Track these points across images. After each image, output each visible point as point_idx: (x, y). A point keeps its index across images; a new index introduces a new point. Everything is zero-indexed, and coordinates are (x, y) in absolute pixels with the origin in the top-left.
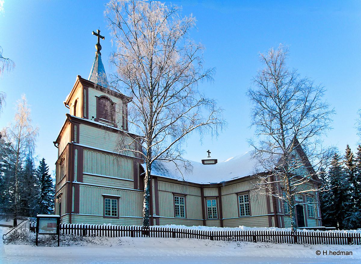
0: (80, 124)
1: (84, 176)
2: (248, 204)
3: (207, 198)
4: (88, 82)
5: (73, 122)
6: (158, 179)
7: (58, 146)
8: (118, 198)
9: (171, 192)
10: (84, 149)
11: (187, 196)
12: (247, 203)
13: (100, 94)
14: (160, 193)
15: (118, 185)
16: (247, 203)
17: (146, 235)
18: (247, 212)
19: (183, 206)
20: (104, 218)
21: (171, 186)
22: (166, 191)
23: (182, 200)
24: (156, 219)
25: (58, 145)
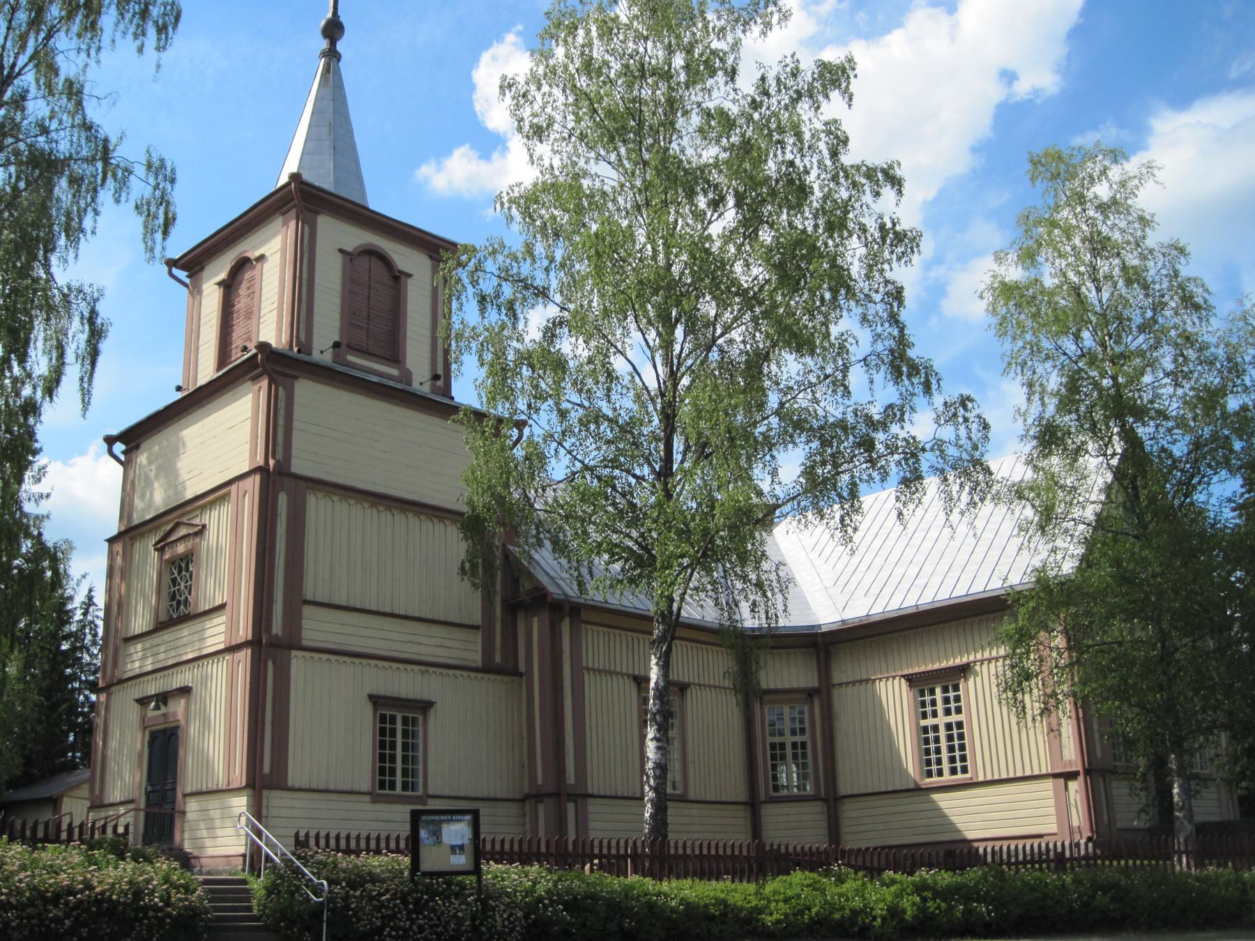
0: (296, 378)
1: (307, 611)
2: (924, 716)
3: (766, 697)
4: (319, 193)
5: (274, 371)
6: (585, 615)
7: (122, 458)
8: (425, 706)
9: (628, 676)
10: (308, 491)
11: (689, 691)
12: (930, 722)
13: (356, 237)
14: (590, 682)
15: (429, 643)
16: (930, 722)
17: (783, 850)
18: (952, 760)
19: (804, 745)
20: (373, 802)
21: (607, 639)
22: (605, 672)
23: (931, 735)
24: (575, 802)
25: (124, 452)
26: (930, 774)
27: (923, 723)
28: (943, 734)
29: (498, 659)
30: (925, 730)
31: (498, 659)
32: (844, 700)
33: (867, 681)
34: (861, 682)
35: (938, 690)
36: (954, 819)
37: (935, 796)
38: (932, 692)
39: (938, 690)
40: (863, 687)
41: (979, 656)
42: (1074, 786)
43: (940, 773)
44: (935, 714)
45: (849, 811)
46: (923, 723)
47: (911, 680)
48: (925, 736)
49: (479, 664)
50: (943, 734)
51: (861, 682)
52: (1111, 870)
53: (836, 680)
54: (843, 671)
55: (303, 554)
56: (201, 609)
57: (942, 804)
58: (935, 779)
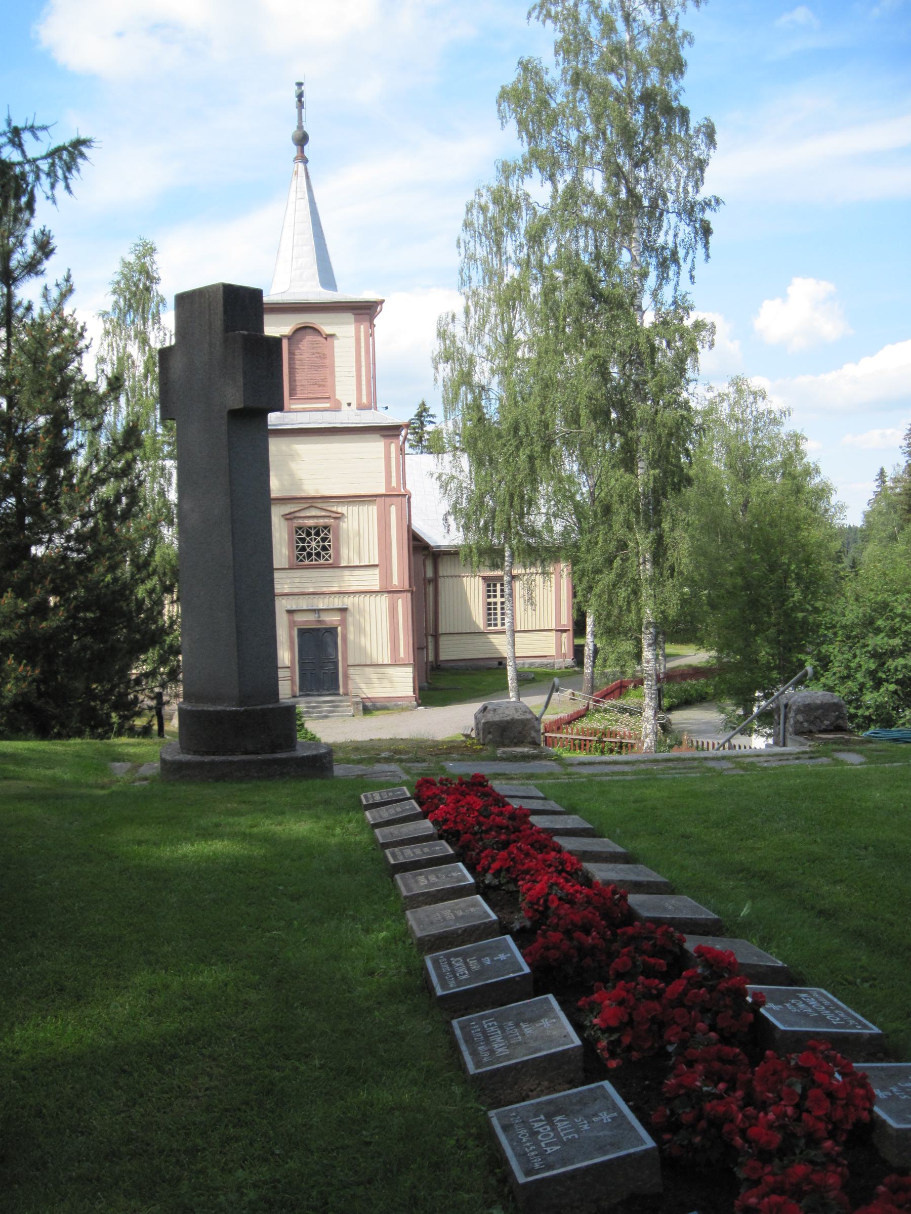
2: (489, 597)
16: (492, 600)
26: (490, 625)
27: (489, 600)
28: (499, 606)
29: (395, 581)
30: (489, 604)
31: (395, 581)
32: (445, 586)
33: (460, 576)
34: (456, 576)
35: (498, 585)
36: (498, 647)
37: (490, 636)
38: (495, 585)
39: (498, 585)
40: (455, 579)
41: (523, 571)
42: (564, 635)
43: (496, 625)
44: (495, 596)
45: (443, 641)
46: (489, 600)
47: (484, 578)
48: (490, 609)
49: (377, 588)
50: (499, 606)
51: (456, 576)
52: (769, 749)
53: (441, 574)
54: (445, 569)
55: (330, 263)
56: (342, 565)
57: (493, 640)
58: (493, 628)
